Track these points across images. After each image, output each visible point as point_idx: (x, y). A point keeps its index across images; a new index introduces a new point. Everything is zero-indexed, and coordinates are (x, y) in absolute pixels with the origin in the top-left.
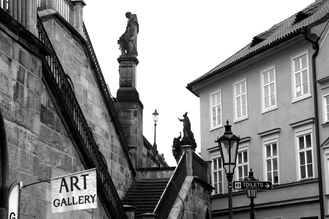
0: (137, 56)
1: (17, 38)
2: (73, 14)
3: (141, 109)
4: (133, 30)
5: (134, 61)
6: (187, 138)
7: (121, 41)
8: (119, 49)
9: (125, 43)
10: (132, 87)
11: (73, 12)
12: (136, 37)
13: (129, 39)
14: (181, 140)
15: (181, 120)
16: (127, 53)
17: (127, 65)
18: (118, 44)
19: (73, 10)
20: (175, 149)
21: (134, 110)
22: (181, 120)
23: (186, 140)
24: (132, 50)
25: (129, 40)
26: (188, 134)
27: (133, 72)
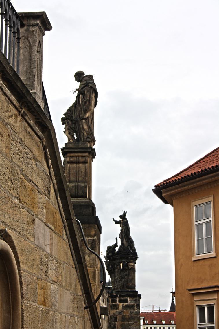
0: (94, 144)
1: (16, 103)
2: (18, 50)
3: (100, 233)
4: (90, 101)
5: (89, 153)
6: (126, 247)
7: (69, 119)
8: (65, 132)
9: (74, 122)
10: (87, 197)
11: (19, 43)
12: (93, 114)
13: (81, 116)
14: (117, 249)
15: (117, 222)
16: (78, 140)
17: (79, 160)
18: (63, 124)
19: (19, 39)
20: (109, 261)
21: (89, 238)
22: (117, 222)
23: (124, 250)
24: (85, 134)
25: (81, 118)
26: (127, 241)
27: (87, 172)
